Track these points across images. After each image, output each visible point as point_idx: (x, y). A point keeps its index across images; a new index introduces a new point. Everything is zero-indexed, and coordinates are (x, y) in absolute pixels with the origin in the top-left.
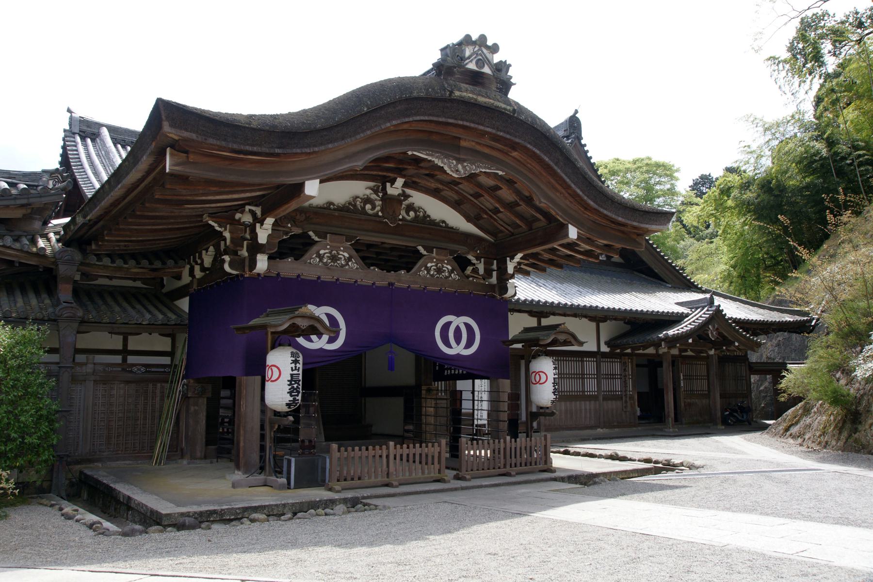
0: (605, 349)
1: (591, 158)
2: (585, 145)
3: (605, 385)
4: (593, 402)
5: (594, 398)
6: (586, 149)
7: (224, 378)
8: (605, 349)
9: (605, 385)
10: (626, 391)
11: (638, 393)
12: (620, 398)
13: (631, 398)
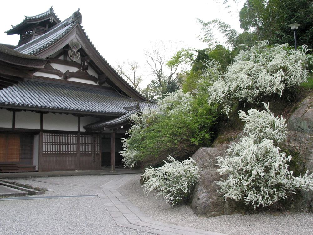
0: (82, 130)
1: (57, 16)
2: (83, 27)
3: (82, 149)
4: (73, 157)
5: (75, 155)
6: (83, 28)
7: (110, 152)
8: (82, 130)
9: (82, 149)
10: (94, 152)
11: (103, 153)
12: (90, 155)
13: (98, 155)
